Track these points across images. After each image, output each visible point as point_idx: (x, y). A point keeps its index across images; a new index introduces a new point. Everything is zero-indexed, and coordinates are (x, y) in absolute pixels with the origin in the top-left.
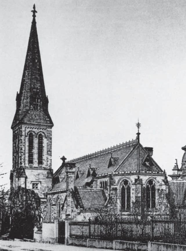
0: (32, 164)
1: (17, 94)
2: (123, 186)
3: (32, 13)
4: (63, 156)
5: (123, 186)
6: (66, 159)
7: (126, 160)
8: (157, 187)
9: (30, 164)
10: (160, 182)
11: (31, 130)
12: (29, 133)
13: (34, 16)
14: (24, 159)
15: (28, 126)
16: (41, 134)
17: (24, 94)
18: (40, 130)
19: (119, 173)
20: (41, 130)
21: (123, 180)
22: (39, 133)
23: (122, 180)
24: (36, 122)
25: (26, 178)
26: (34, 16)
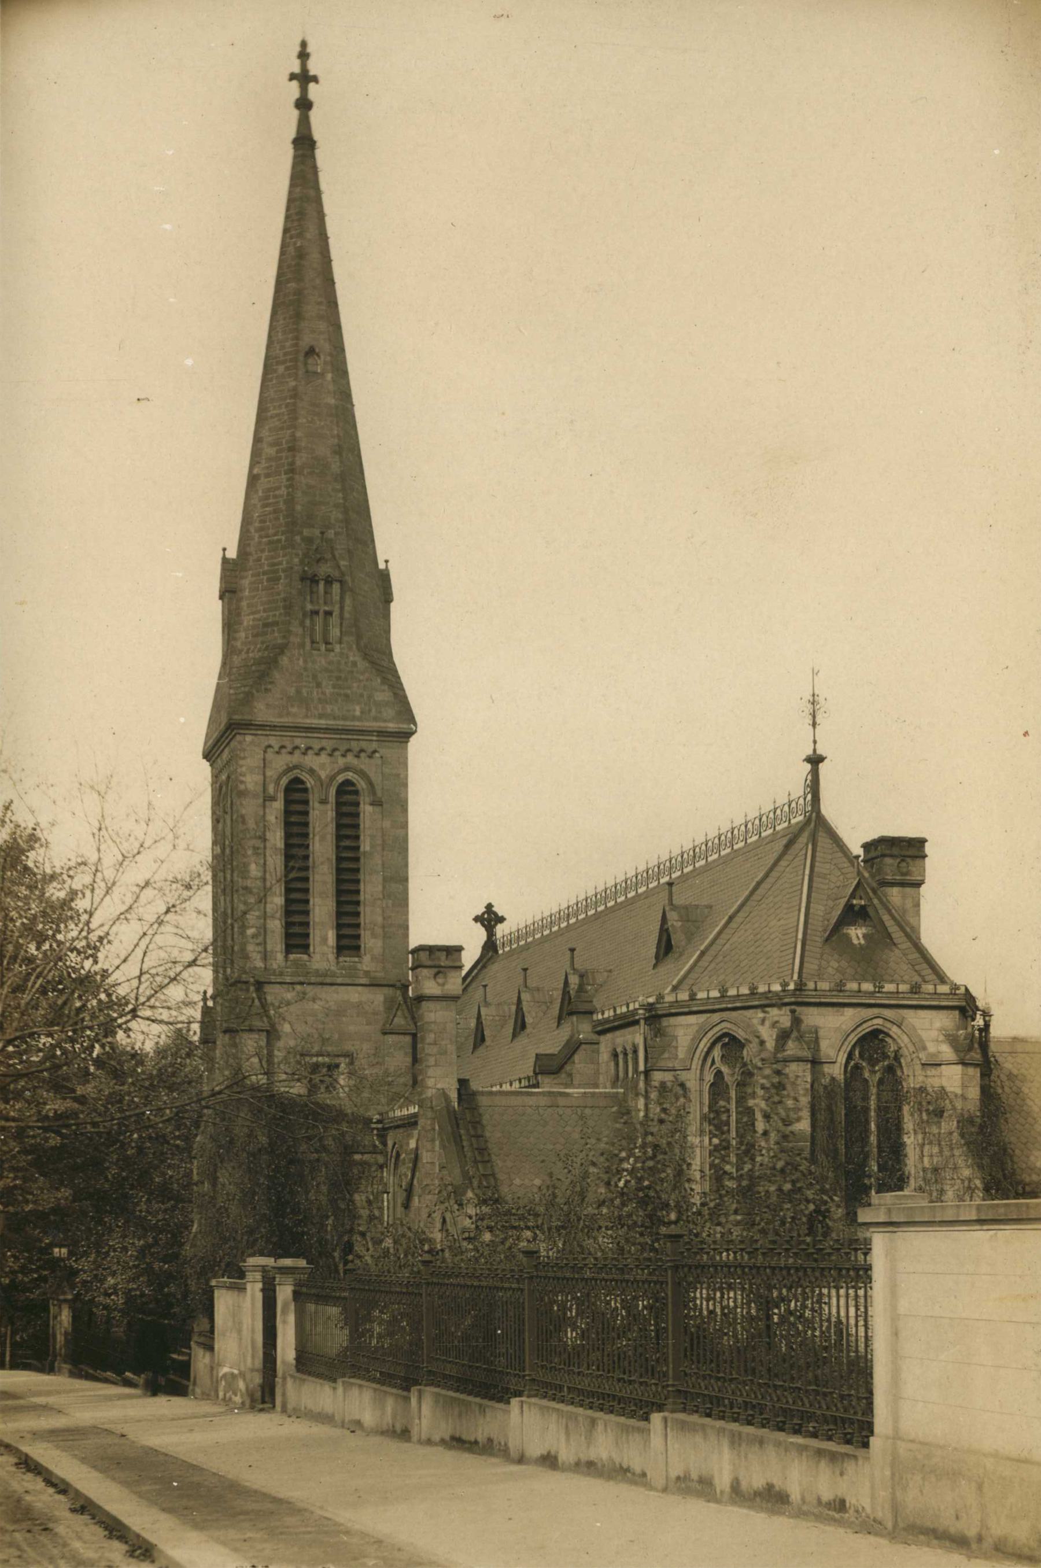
0: (305, 957)
1: (225, 561)
2: (719, 1074)
3: (295, 84)
4: (927, 838)
5: (719, 1074)
6: (501, 920)
7: (738, 919)
8: (913, 1078)
9: (292, 957)
10: (932, 1048)
11: (296, 758)
12: (284, 781)
13: (304, 105)
14: (263, 930)
15: (274, 742)
16: (348, 782)
17: (254, 561)
18: (341, 762)
19: (693, 997)
20: (350, 759)
21: (718, 1039)
22: (340, 778)
23: (710, 1034)
24: (321, 716)
25: (272, 1034)
26: (304, 105)
